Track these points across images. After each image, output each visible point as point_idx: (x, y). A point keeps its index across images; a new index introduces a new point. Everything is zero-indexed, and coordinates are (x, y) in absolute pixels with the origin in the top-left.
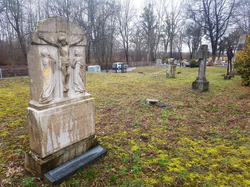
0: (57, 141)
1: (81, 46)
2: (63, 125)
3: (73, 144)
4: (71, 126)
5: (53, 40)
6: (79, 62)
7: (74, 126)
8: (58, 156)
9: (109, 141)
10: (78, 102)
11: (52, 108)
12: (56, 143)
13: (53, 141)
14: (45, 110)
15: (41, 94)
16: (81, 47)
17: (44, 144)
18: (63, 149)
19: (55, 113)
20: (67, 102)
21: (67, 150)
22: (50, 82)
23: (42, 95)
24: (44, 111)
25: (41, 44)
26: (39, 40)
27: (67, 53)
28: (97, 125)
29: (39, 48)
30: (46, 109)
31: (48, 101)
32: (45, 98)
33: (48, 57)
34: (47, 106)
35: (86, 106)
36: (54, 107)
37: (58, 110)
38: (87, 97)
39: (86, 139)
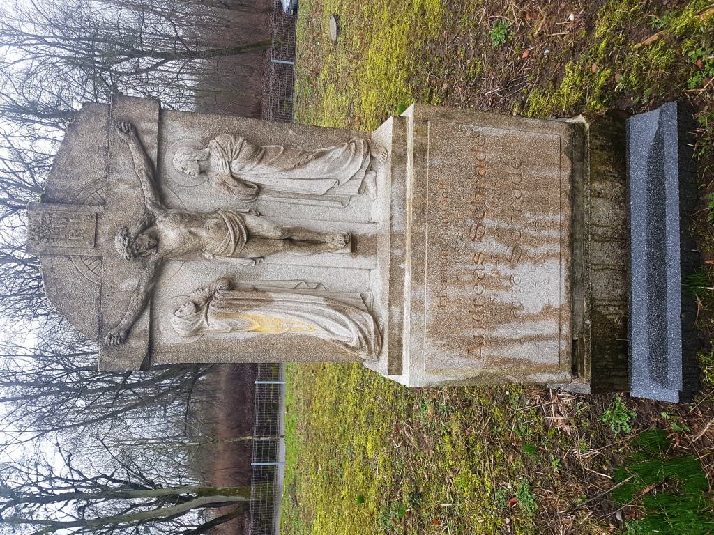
0: (535, 318)
1: (164, 131)
2: (480, 288)
3: (572, 247)
4: (501, 249)
5: (131, 282)
6: (235, 166)
7: (499, 234)
8: (589, 322)
9: (628, 33)
10: (409, 194)
11: (405, 320)
12: (541, 323)
13: (526, 338)
14: (404, 352)
15: (343, 347)
16: (169, 137)
17: (526, 373)
18: (572, 297)
19: (426, 316)
20: (397, 252)
21: (583, 274)
22: (301, 320)
23: (347, 346)
24: (409, 365)
25: (151, 334)
26: (133, 343)
27: (190, 232)
28: (525, 13)
29: (167, 342)
30: (401, 346)
31: (372, 333)
32: (360, 342)
33: (203, 317)
34: (390, 344)
35: (437, 161)
36: (402, 313)
37: (417, 305)
38: (399, 140)
39: (572, 179)
